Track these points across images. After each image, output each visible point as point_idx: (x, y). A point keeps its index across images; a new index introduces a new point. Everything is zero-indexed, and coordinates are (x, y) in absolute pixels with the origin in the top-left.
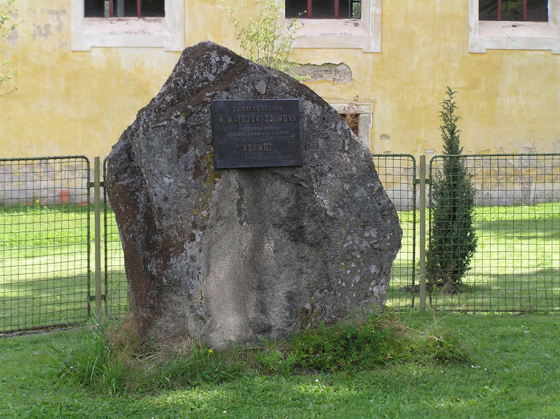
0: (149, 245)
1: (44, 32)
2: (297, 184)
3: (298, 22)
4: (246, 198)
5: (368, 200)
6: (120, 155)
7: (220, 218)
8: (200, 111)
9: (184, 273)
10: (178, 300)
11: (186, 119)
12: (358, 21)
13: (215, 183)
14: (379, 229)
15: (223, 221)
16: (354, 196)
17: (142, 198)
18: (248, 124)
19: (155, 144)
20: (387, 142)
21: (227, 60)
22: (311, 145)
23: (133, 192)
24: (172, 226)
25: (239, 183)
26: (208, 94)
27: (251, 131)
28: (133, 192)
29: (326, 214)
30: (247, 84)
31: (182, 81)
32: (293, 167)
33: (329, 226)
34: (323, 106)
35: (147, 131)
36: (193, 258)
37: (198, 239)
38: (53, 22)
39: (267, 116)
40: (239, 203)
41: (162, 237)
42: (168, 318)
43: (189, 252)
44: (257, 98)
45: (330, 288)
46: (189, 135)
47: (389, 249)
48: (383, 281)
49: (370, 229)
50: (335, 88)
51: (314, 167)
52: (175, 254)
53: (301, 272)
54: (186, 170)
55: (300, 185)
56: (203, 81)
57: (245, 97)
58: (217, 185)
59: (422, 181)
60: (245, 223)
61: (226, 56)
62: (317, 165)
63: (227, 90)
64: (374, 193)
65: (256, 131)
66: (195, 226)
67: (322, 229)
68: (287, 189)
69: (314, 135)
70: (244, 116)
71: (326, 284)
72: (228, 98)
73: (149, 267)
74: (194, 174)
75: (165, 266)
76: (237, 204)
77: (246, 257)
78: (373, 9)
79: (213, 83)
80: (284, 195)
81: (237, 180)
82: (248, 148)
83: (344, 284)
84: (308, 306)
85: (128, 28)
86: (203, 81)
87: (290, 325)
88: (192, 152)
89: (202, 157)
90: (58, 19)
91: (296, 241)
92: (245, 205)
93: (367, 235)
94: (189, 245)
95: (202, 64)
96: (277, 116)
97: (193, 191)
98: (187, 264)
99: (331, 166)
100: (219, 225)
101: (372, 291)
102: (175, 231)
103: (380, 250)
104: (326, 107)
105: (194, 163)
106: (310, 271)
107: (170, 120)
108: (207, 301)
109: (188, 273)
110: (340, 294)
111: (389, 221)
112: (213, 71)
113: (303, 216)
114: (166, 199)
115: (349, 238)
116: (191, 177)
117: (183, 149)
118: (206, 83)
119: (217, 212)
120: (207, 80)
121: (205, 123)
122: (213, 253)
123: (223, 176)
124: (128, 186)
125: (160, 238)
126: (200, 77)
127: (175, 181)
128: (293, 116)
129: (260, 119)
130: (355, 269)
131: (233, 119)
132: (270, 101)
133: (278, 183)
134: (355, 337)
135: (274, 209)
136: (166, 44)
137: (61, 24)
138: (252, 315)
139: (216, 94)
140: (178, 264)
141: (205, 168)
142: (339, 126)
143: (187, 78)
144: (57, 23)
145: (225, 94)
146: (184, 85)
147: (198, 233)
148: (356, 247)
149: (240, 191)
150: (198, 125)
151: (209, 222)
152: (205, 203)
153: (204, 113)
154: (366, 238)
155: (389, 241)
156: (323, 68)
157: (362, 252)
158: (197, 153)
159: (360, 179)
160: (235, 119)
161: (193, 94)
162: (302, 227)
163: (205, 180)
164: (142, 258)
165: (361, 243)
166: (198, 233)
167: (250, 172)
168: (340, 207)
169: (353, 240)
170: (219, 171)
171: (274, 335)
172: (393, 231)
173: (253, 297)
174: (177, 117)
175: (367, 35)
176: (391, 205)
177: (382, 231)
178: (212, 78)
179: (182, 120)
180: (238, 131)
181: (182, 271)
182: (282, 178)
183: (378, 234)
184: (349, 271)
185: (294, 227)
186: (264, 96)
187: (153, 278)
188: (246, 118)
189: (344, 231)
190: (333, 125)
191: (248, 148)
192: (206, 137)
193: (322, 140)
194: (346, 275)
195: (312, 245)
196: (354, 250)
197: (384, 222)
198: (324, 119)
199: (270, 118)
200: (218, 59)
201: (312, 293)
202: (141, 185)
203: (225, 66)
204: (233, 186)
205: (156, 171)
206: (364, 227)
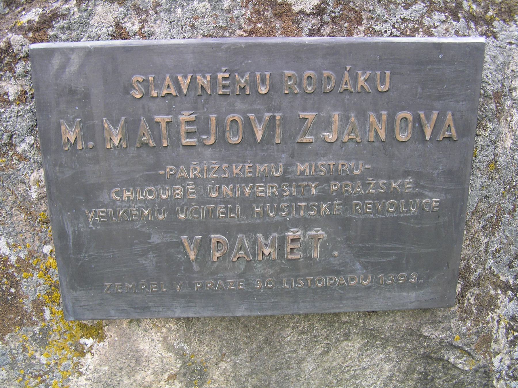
18: (208, 152)
25: (180, 354)
27: (221, 182)
39: (310, 115)
44: (271, 33)
57: (205, 25)
58: (89, 361)
65: (254, 180)
68: (387, 367)
70: (185, 116)
72: (120, 32)
81: (169, 348)
82: (204, 247)
96: (362, 116)
128: (440, 120)
131: (131, 131)
132: (332, 51)
141: (38, 305)
160: (144, 127)
180: (158, 180)
186: (307, 25)
188: (200, 127)
191: (204, 247)
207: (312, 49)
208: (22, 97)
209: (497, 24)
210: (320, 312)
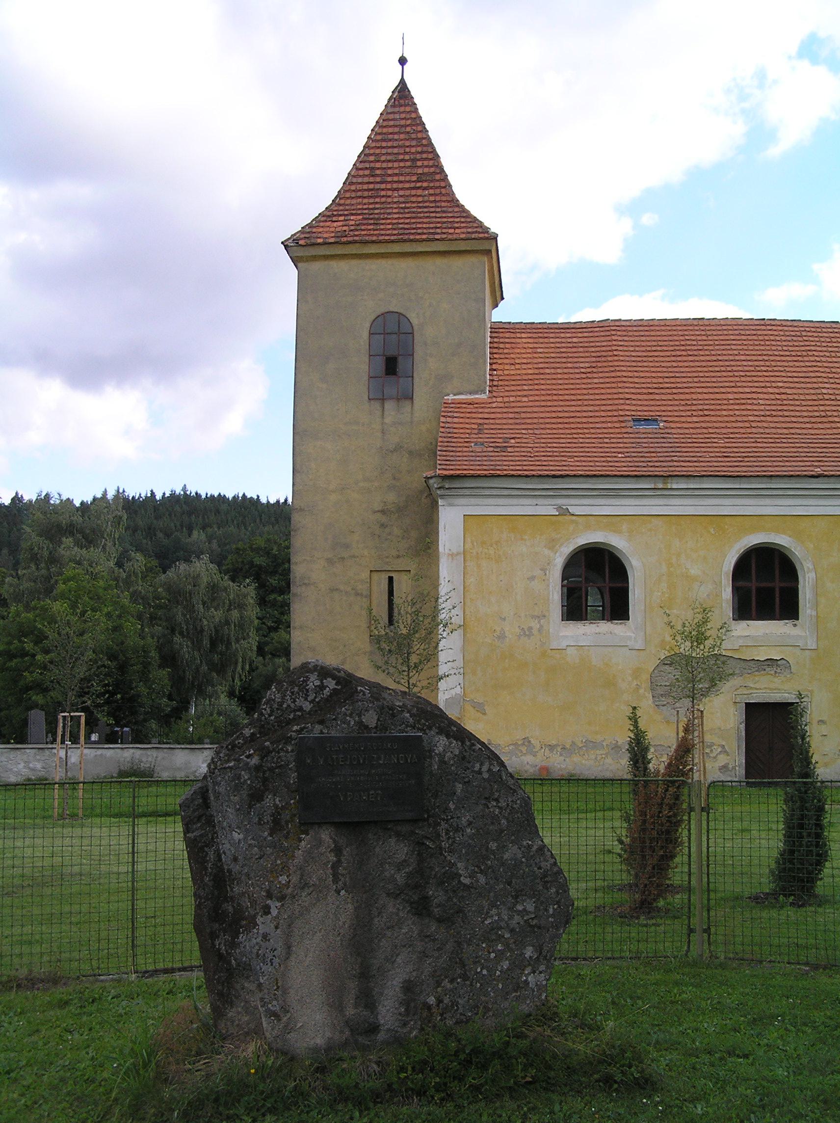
0: (217, 915)
1: (527, 633)
2: (418, 843)
3: (743, 624)
4: (346, 859)
5: (522, 862)
6: (193, 800)
7: (306, 885)
8: (282, 749)
9: (254, 956)
10: (251, 988)
11: (262, 759)
12: (796, 622)
13: (300, 840)
14: (538, 899)
15: (311, 889)
16: (502, 858)
17: (211, 856)
19: (222, 789)
20: (823, 726)
21: (331, 684)
22: (444, 792)
23: (202, 848)
24: (243, 893)
25: (334, 841)
26: (295, 728)
28: (202, 848)
29: (460, 881)
30: (351, 715)
31: (268, 710)
32: (415, 821)
33: (463, 897)
34: (463, 743)
35: (214, 773)
36: (265, 937)
37: (274, 912)
38: (535, 624)
40: (335, 867)
41: (233, 906)
42: (240, 1009)
43: (262, 929)
44: (363, 733)
45: (465, 977)
46: (265, 780)
47: (552, 927)
48: (542, 968)
49: (524, 901)
50: (776, 680)
51: (447, 820)
52: (246, 930)
53: (424, 955)
54: (260, 824)
55: (423, 844)
56: (295, 711)
59: (698, 809)
60: (343, 892)
61: (329, 679)
62: (452, 818)
63: (321, 722)
64: (532, 854)
66: (269, 896)
67: (455, 900)
68: (406, 849)
69: (448, 780)
71: (459, 971)
72: (322, 733)
73: (217, 943)
74: (270, 829)
75: (233, 945)
76: (333, 867)
77: (344, 936)
78: (809, 611)
79: (309, 713)
80: (401, 856)
81: (331, 838)
83: (485, 972)
84: (432, 1000)
85: (598, 630)
86: (295, 711)
87: (405, 1025)
88: (270, 801)
89: (283, 808)
90: (539, 622)
91: (419, 914)
92: (345, 869)
93: (520, 907)
94: (261, 919)
95: (296, 689)
97: (269, 850)
98: (257, 943)
99: (471, 819)
100: (304, 894)
101: (526, 981)
102: (247, 900)
103: (539, 928)
104: (468, 743)
105: (273, 815)
106: (436, 954)
107: (238, 760)
108: (285, 992)
109: (258, 955)
110: (478, 985)
111: (553, 890)
112: (309, 699)
113: (427, 883)
114: (235, 859)
115: (494, 911)
116: (266, 833)
117: (256, 797)
118: (299, 713)
119: (301, 879)
120: (300, 709)
121: (288, 765)
122: (295, 930)
123: (311, 832)
124: (195, 839)
125: (230, 907)
126: (292, 705)
127: (245, 838)
129: (364, 759)
130: (502, 952)
132: (380, 737)
133: (393, 841)
134: (476, 1051)
135: (387, 874)
136: (629, 643)
137: (541, 626)
138: (350, 1011)
139: (304, 728)
140: (249, 942)
142: (485, 768)
143: (276, 706)
144: (538, 626)
145: (318, 727)
146: (270, 716)
147: (274, 905)
148: (503, 924)
149: (338, 851)
150: (277, 767)
151: (290, 890)
152: (285, 868)
153: (287, 751)
154: (519, 913)
155: (553, 916)
156: (766, 663)
157: (512, 931)
158: (278, 802)
159: (513, 835)
161: (282, 727)
162: (427, 898)
163: (286, 838)
164: (208, 931)
165: (511, 918)
166: (274, 905)
167: (353, 827)
168: (481, 872)
169: (499, 914)
170: (306, 826)
171: (381, 1036)
172: (558, 903)
173: (353, 987)
174: (248, 757)
175: (804, 634)
176: (555, 869)
177: (542, 903)
178: (307, 706)
179: (255, 761)
181: (251, 952)
182: (398, 834)
183: (536, 907)
184: (493, 955)
185: (416, 898)
187: (220, 956)
189: (485, 904)
190: (477, 766)
192: (289, 783)
193: (461, 785)
194: (488, 960)
195: (440, 921)
196: (501, 928)
197: (546, 891)
198: (464, 758)
199: (379, 758)
200: (317, 683)
201: (438, 984)
202: (213, 838)
203: (327, 692)
204: (326, 845)
205: (225, 823)
206: (516, 897)
207: (375, 737)
208: (292, 751)
209: (427, 731)
210: (379, 435)
